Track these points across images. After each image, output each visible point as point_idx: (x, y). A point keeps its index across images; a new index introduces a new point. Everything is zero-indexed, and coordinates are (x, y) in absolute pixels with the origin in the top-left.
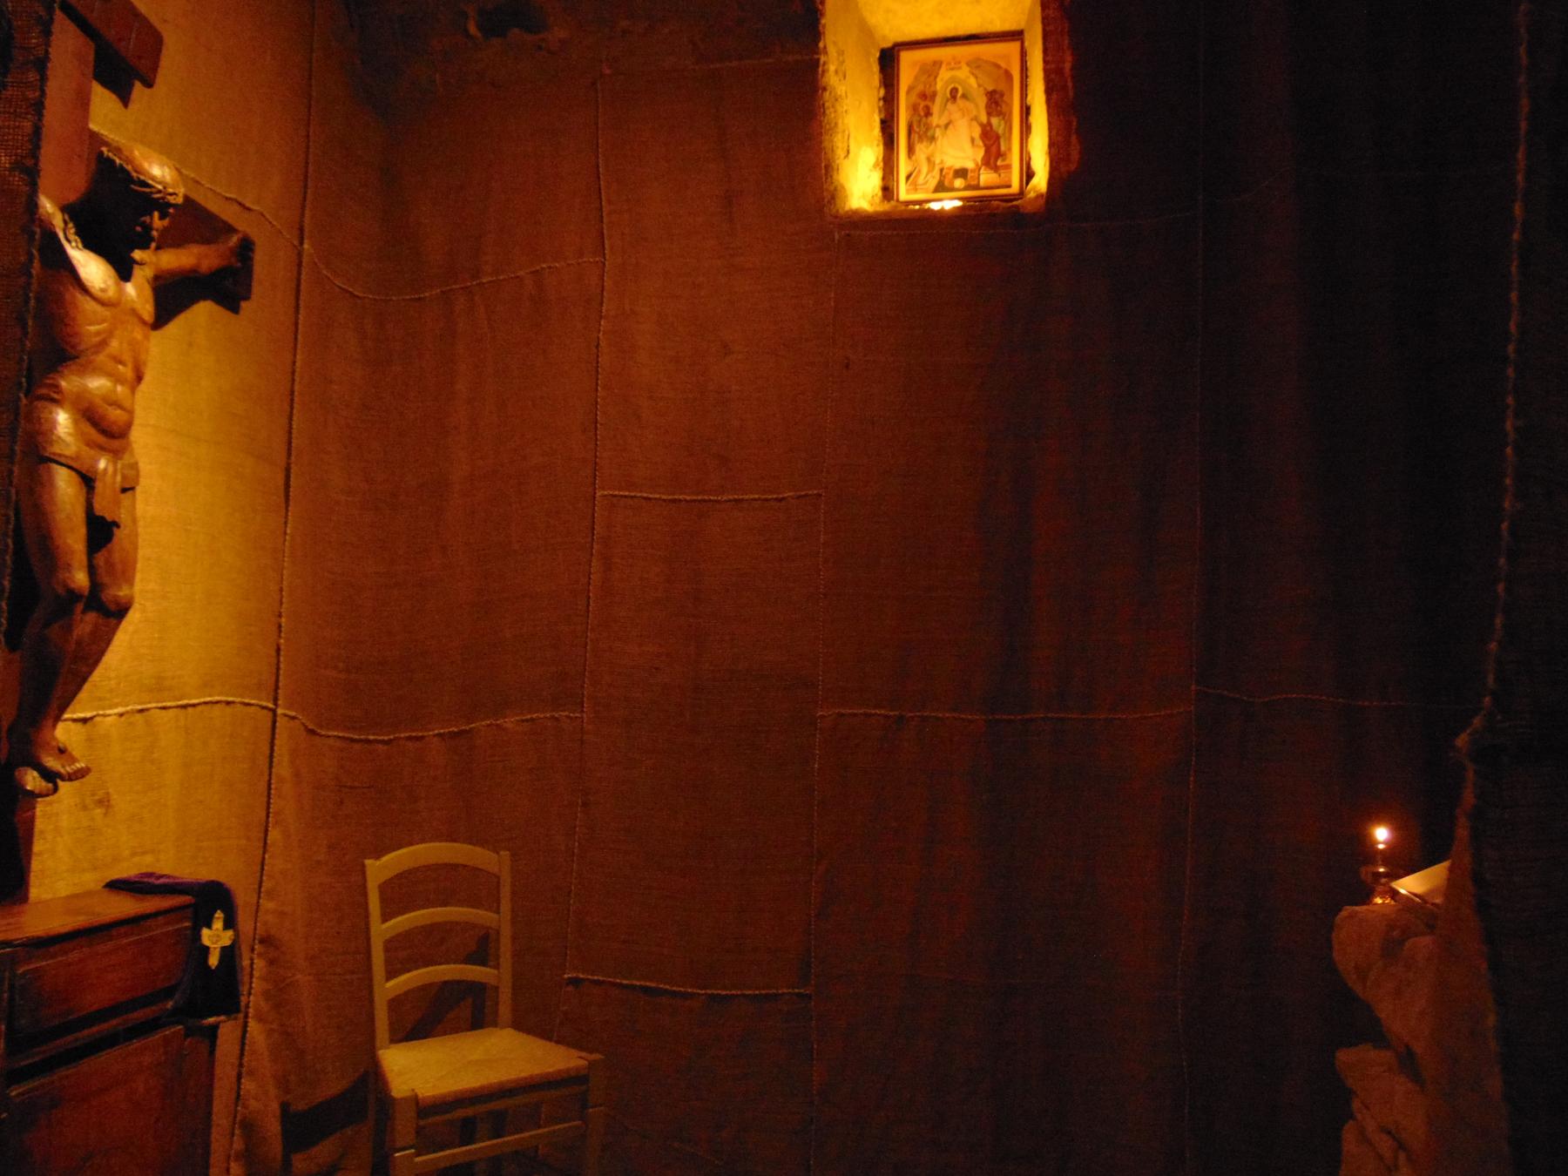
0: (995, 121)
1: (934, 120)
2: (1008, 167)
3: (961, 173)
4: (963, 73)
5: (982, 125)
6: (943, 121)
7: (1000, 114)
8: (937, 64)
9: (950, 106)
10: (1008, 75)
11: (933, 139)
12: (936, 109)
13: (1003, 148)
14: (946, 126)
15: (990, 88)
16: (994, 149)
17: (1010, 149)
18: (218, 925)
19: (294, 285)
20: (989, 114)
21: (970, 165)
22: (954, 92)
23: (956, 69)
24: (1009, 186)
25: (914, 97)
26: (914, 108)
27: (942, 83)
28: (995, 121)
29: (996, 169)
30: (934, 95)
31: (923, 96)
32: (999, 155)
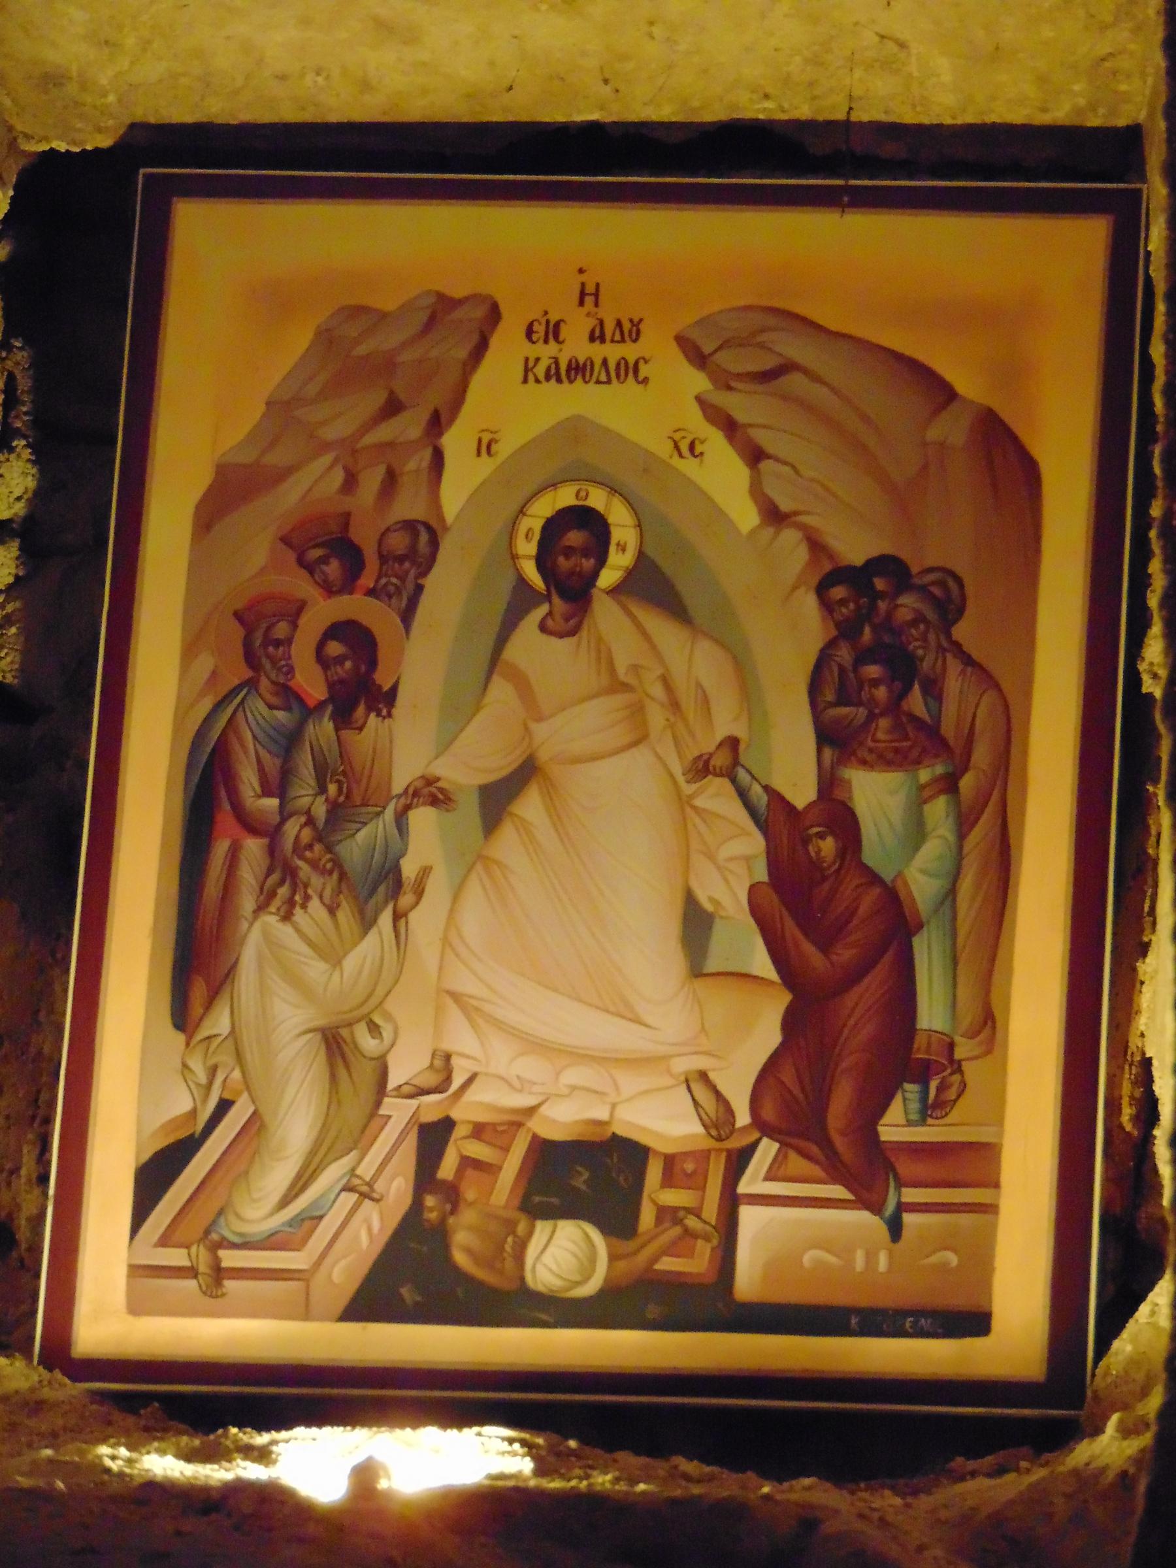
0: (878, 796)
1: (406, 744)
2: (971, 1165)
3: (590, 1175)
4: (655, 408)
5: (775, 817)
6: (470, 764)
7: (920, 743)
8: (464, 323)
9: (529, 645)
10: (1005, 462)
11: (382, 888)
12: (422, 662)
13: (932, 1014)
14: (497, 801)
15: (855, 548)
16: (858, 1013)
17: (988, 1024)
18: (609, 1477)
19: (999, 821)
20: (837, 741)
21: (664, 1120)
22: (575, 537)
23: (600, 378)
24: (976, 1322)
25: (254, 553)
26: (254, 634)
27: (487, 463)
28: (878, 796)
29: (867, 1173)
30: (421, 544)
31: (330, 548)
32: (905, 1060)
